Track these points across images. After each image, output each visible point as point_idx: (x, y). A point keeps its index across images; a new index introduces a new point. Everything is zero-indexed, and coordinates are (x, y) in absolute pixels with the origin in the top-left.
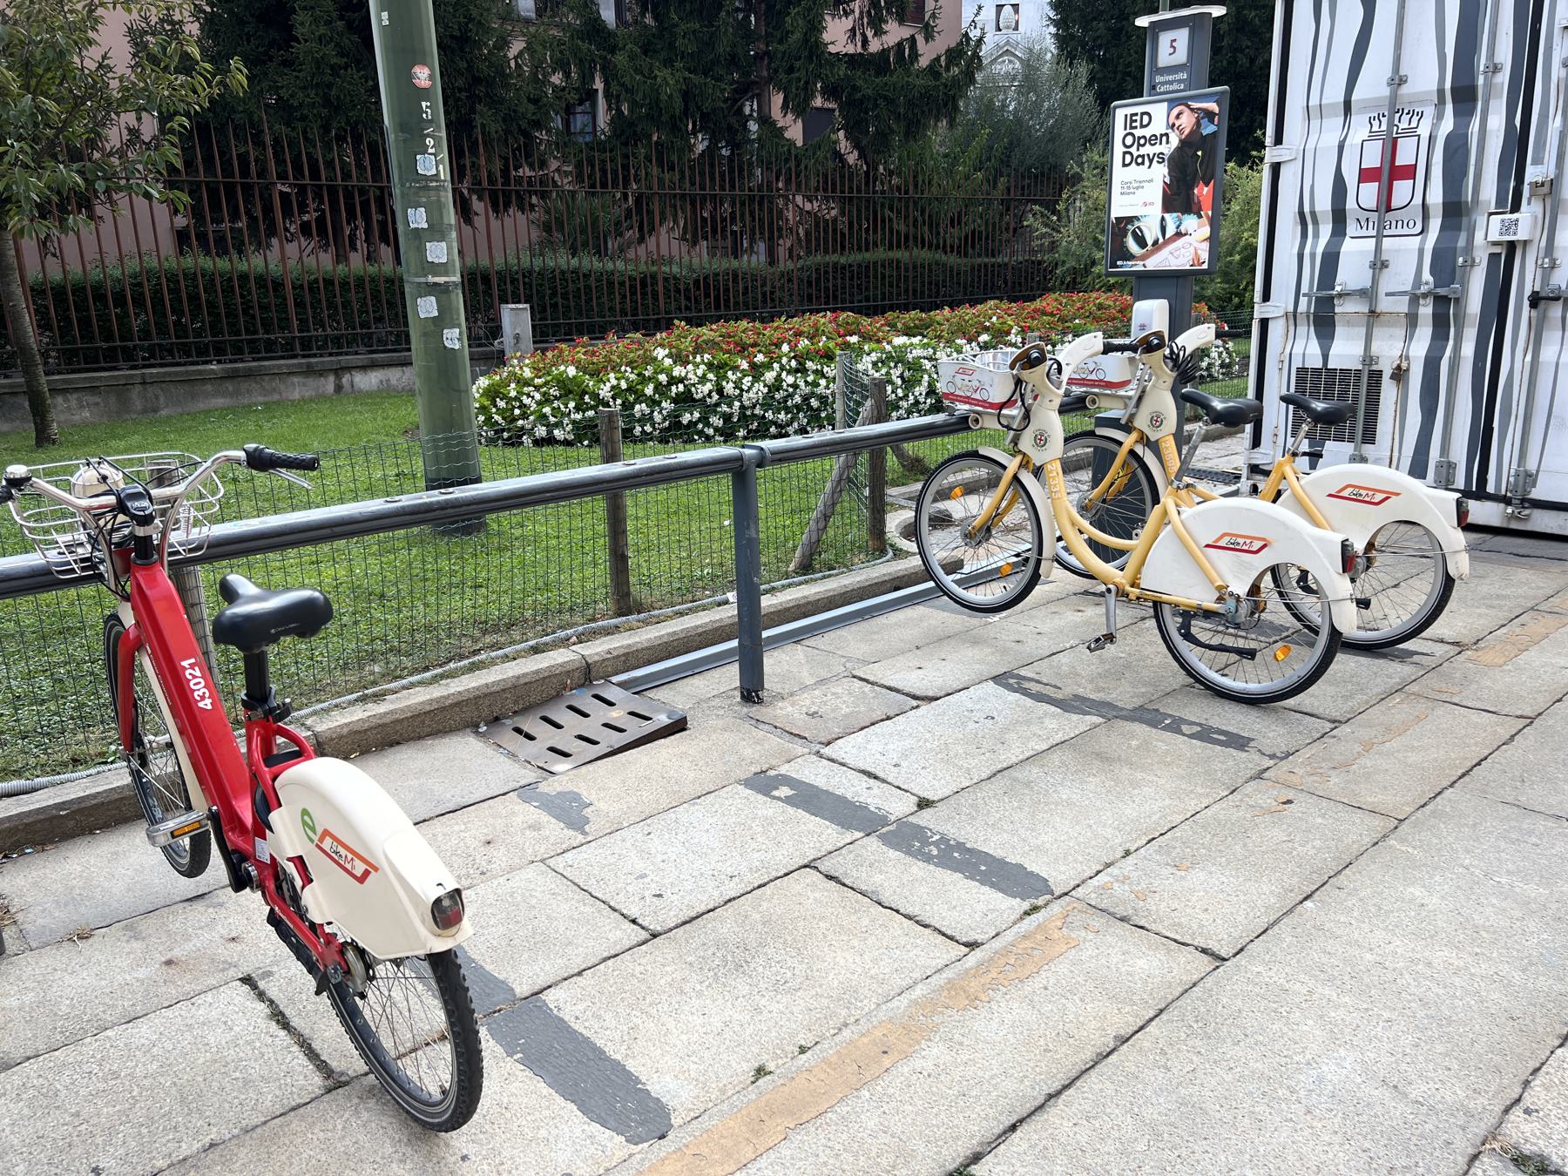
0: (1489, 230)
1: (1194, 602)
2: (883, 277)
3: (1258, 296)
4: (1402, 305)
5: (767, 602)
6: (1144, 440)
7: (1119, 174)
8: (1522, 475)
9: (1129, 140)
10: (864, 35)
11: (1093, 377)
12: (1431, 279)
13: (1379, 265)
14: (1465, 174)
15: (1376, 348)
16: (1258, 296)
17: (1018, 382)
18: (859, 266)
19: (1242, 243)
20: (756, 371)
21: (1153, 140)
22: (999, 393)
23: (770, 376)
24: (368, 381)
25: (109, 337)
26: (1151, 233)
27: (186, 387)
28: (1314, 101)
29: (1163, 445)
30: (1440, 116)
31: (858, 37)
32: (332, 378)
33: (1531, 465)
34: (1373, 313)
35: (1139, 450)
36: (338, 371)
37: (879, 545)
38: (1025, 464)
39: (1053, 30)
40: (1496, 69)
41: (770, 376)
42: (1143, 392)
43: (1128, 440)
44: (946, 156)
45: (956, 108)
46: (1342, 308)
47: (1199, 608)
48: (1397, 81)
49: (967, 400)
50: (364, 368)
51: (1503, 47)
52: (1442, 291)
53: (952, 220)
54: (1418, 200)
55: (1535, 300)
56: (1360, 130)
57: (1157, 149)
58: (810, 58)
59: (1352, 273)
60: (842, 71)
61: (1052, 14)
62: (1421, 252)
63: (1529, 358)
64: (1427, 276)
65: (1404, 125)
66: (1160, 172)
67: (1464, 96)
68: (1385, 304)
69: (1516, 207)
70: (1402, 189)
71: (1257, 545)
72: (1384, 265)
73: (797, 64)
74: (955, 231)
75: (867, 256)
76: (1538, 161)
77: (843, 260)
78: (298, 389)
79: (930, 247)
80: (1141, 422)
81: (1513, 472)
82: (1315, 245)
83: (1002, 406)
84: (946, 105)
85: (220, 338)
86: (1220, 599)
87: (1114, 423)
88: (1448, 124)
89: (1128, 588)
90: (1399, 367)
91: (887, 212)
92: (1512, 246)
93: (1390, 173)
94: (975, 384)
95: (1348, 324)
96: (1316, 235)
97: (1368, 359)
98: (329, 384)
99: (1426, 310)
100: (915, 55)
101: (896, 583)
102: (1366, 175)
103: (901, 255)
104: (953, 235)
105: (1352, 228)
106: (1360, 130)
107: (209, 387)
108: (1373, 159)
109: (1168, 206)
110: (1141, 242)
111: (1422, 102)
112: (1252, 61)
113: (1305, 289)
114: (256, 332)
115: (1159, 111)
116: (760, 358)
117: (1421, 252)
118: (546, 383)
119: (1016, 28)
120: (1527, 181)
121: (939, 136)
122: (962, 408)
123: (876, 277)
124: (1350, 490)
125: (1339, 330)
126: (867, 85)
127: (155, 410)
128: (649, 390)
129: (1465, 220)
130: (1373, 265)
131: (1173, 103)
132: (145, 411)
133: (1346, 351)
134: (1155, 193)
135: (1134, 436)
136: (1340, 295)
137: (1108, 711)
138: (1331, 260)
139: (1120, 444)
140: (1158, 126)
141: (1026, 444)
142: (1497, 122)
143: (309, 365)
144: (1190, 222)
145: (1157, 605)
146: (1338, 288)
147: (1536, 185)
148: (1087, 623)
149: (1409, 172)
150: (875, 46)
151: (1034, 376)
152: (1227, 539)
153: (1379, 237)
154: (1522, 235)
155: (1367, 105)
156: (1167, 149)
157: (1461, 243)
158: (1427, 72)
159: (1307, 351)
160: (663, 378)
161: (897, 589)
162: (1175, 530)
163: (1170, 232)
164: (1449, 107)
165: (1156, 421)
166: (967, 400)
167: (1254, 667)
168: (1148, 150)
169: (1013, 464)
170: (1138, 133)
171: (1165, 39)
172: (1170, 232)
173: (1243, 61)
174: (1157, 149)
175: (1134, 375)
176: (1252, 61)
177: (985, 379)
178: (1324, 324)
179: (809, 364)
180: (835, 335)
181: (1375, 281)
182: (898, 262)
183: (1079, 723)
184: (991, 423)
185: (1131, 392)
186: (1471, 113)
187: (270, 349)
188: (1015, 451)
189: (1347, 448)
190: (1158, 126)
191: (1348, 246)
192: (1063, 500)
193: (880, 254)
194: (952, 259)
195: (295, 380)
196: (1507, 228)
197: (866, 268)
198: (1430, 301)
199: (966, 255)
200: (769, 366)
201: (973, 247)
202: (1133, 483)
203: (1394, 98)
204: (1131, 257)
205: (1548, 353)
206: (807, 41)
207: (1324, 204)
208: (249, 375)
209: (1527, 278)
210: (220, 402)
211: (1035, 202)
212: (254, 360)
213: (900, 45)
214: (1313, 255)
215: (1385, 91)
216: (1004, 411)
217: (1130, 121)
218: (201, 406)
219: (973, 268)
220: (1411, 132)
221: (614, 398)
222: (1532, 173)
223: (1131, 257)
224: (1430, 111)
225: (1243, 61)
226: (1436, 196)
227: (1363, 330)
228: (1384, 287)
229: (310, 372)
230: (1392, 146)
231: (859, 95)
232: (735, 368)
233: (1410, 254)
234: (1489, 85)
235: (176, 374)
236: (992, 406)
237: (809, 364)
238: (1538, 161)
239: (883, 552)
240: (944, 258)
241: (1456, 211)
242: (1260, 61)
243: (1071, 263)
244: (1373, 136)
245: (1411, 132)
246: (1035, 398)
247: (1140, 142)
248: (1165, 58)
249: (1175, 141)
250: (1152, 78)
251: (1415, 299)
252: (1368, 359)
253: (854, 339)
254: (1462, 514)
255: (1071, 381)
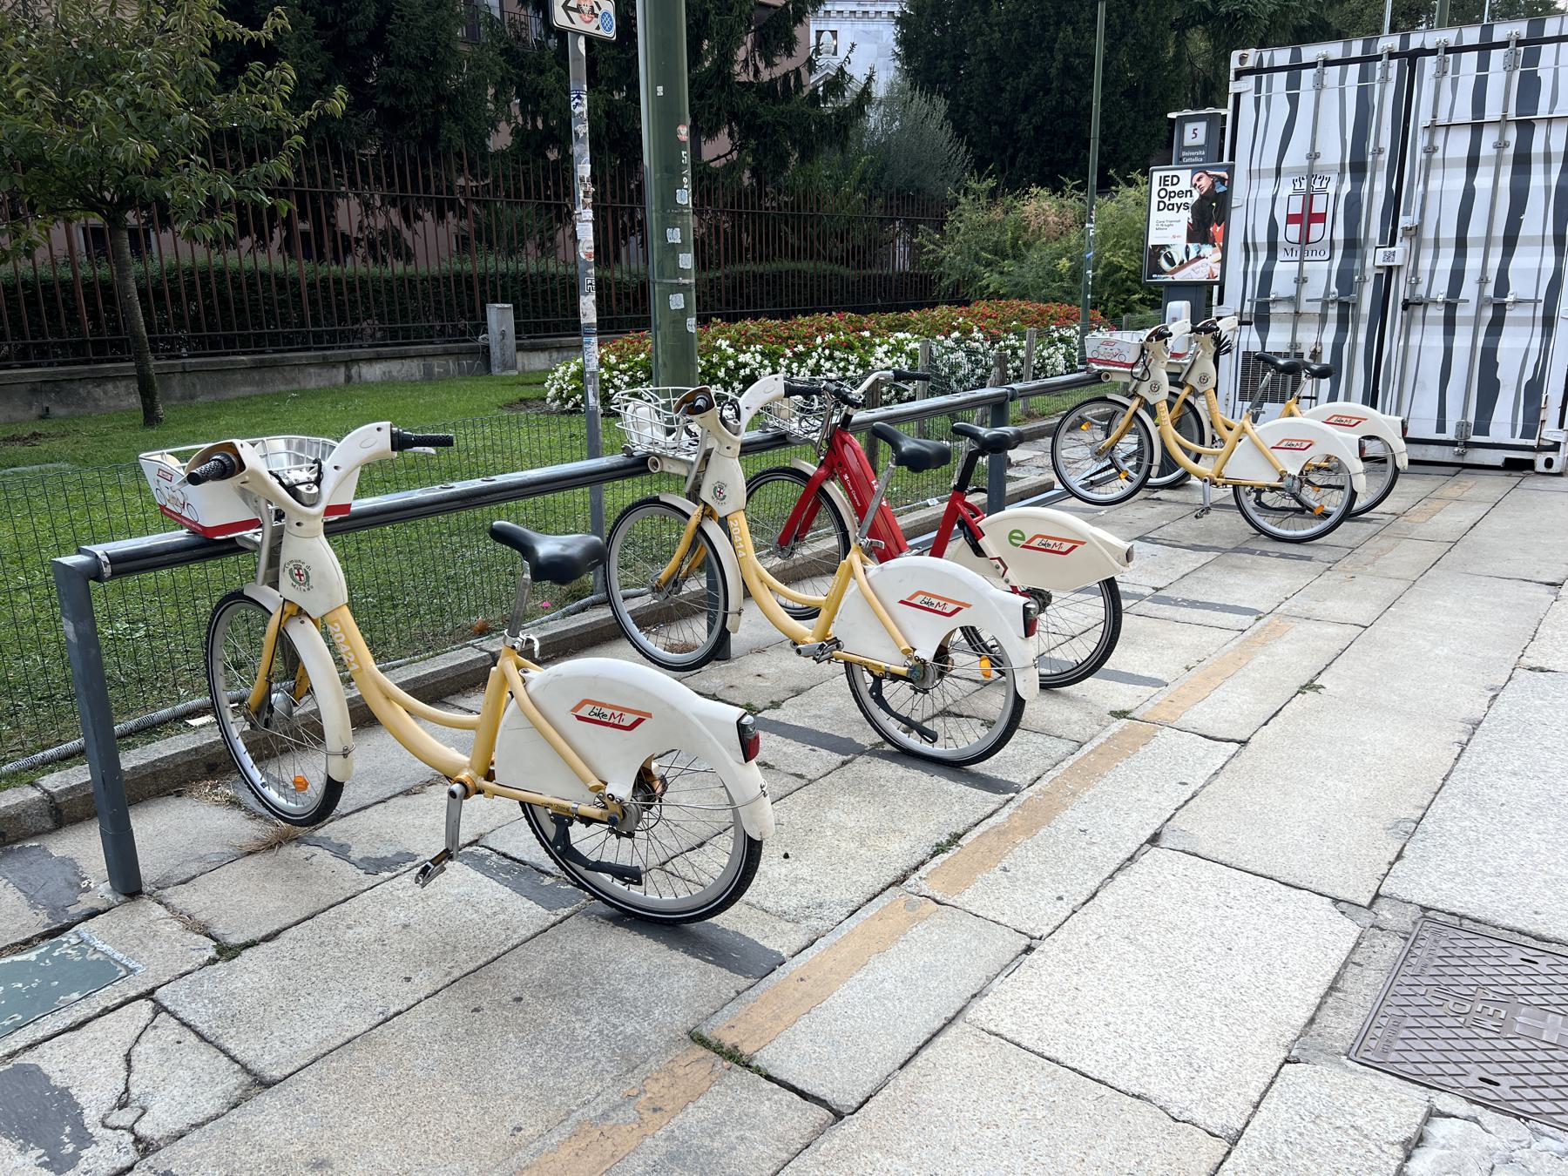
0: (1375, 258)
3: (1215, 301)
5: (130, 760)
7: (1155, 216)
9: (1163, 193)
10: (755, 65)
13: (1301, 280)
14: (1359, 220)
15: (1299, 338)
16: (1215, 301)
19: (1104, 262)
20: (800, 358)
21: (1180, 194)
23: (811, 363)
24: (373, 372)
25: (227, 325)
26: (1179, 256)
27: (219, 376)
28: (1255, 167)
30: (1342, 181)
31: (751, 68)
32: (343, 370)
35: (1191, 399)
36: (348, 363)
38: (708, 513)
39: (898, 63)
40: (1380, 151)
41: (811, 363)
44: (830, 177)
45: (847, 137)
48: (1313, 156)
50: (370, 360)
51: (1384, 137)
54: (1327, 237)
55: (1406, 305)
56: (1286, 189)
57: (1184, 200)
58: (722, 88)
59: (1282, 285)
60: (751, 98)
61: (897, 49)
62: (1330, 272)
64: (1333, 288)
65: (1317, 186)
66: (1186, 216)
67: (1358, 168)
68: (1305, 307)
69: (1393, 244)
70: (1316, 230)
72: (1305, 281)
73: (709, 92)
76: (1407, 213)
78: (314, 379)
82: (1255, 266)
84: (837, 133)
85: (40, 340)
86: (1281, 480)
88: (1347, 187)
92: (1390, 269)
93: (1307, 218)
95: (1280, 321)
96: (1256, 259)
97: (1294, 345)
98: (340, 375)
99: (1333, 312)
100: (799, 85)
102: (1291, 219)
105: (1281, 255)
106: (1286, 189)
107: (238, 376)
108: (1296, 209)
109: (1191, 239)
110: (1171, 261)
111: (1330, 171)
112: (1077, 102)
113: (1248, 296)
114: (101, 334)
115: (1185, 177)
116: (801, 348)
117: (1330, 272)
118: (631, 368)
119: (835, 53)
120: (1401, 225)
121: (826, 164)
122: (1096, 367)
125: (1272, 325)
126: (766, 113)
127: (192, 398)
128: (721, 374)
129: (1358, 251)
130: (1297, 281)
131: (1195, 171)
132: (183, 398)
133: (1278, 339)
134: (1182, 230)
135: (1137, 401)
137: (1225, 551)
138: (1267, 276)
139: (1127, 407)
140: (1184, 184)
142: (1380, 187)
143: (325, 357)
144: (1207, 250)
147: (1405, 229)
149: (1321, 218)
150: (765, 75)
152: (921, 597)
153: (1301, 261)
154: (1397, 262)
155: (1291, 172)
156: (1191, 201)
157: (1357, 266)
158: (1333, 152)
159: (1249, 339)
160: (731, 363)
163: (1193, 255)
164: (1348, 176)
166: (1099, 362)
167: (1298, 518)
168: (1176, 200)
169: (695, 511)
170: (1170, 189)
171: (1189, 128)
172: (1193, 255)
173: (1069, 101)
174: (1184, 200)
176: (1077, 102)
178: (1261, 319)
179: (837, 354)
181: (1298, 291)
183: (1212, 555)
186: (1363, 179)
187: (289, 343)
188: (694, 496)
189: (1278, 407)
190: (1184, 184)
191: (1279, 267)
195: (312, 370)
196: (1387, 257)
197: (778, 276)
198: (1336, 305)
200: (808, 354)
203: (1311, 167)
204: (1164, 272)
205: (1414, 340)
206: (719, 72)
207: (1262, 237)
208: (274, 365)
209: (1400, 290)
210: (246, 390)
212: (275, 352)
213: (786, 76)
214: (1254, 273)
215: (1306, 163)
217: (1164, 180)
218: (232, 394)
220: (1323, 191)
222: (1403, 221)
223: (1164, 272)
224: (1334, 178)
225: (1069, 101)
226: (1339, 235)
227: (1291, 326)
228: (1305, 295)
229: (326, 363)
230: (1309, 199)
231: (759, 122)
232: (784, 356)
233: (1321, 273)
234: (1375, 161)
235: (212, 364)
236: (1127, 365)
237: (837, 354)
238: (1407, 213)
241: (1353, 245)
242: (1084, 102)
243: (955, 276)
244: (1296, 192)
245: (1323, 191)
247: (1170, 195)
248: (1189, 140)
249: (1196, 195)
250: (1179, 153)
251: (1325, 304)
252: (1294, 345)
254: (1362, 449)
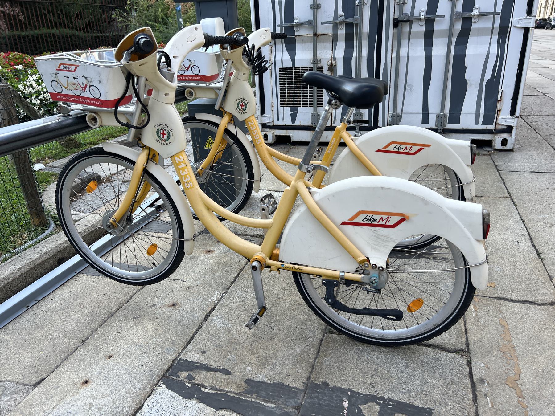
1: (337, 274)
2: (47, 42)
4: (329, 29)
6: (233, 120)
8: (396, 117)
11: (189, 73)
12: (343, 14)
17: (129, 77)
18: (33, 36)
22: (112, 90)
29: (249, 124)
33: (399, 111)
34: (315, 34)
35: (232, 129)
37: (39, 221)
42: (228, 83)
43: (223, 122)
46: (300, 32)
47: (342, 278)
49: (78, 99)
52: (350, 20)
53: (77, 16)
63: (394, 55)
64: (341, 12)
68: (321, 29)
71: (394, 220)
74: (80, 21)
75: (36, 31)
77: (23, 34)
79: (69, 27)
80: (231, 107)
81: (390, 115)
83: (117, 103)
87: (209, 109)
89: (269, 262)
90: (331, 64)
91: (43, 11)
94: (81, 80)
95: (303, 42)
97: (316, 60)
99: (342, 32)
101: (59, 257)
103: (55, 31)
104: (81, 23)
113: (278, 22)
122: (76, 108)
123: (43, 42)
124: (393, 146)
125: (298, 46)
135: (226, 119)
136: (298, 25)
139: (217, 125)
141: (149, 137)
145: (297, 276)
146: (296, 21)
148: (220, 265)
151: (145, 67)
161: (60, 262)
162: (310, 210)
165: (242, 105)
166: (78, 99)
175: (220, 71)
177: (91, 74)
180: (7, 65)
182: (54, 34)
184: (109, 122)
185: (220, 84)
192: (179, 168)
193: (45, 31)
194: (81, 34)
198: (343, 26)
199: (88, 32)
201: (91, 29)
202: (227, 153)
211: (117, 7)
216: (121, 109)
219: (92, 38)
221: (41, 100)
227: (311, 45)
228: (320, 20)
236: (105, 104)
239: (45, 225)
240: (77, 33)
246: (149, 93)
251: (336, 26)
252: (316, 60)
253: (20, 67)
255: (181, 78)
